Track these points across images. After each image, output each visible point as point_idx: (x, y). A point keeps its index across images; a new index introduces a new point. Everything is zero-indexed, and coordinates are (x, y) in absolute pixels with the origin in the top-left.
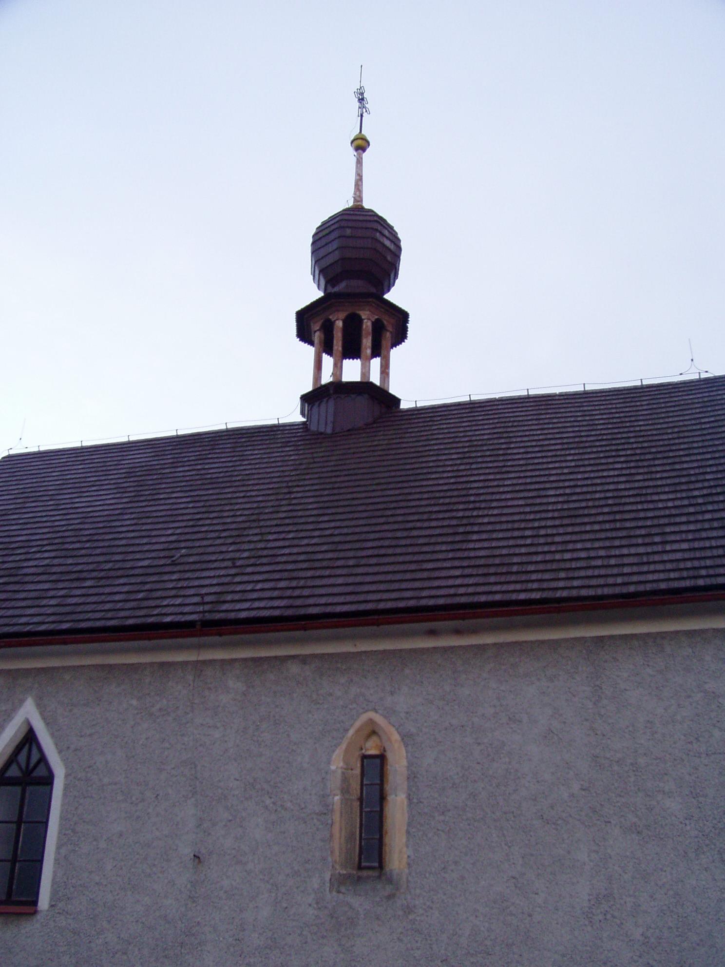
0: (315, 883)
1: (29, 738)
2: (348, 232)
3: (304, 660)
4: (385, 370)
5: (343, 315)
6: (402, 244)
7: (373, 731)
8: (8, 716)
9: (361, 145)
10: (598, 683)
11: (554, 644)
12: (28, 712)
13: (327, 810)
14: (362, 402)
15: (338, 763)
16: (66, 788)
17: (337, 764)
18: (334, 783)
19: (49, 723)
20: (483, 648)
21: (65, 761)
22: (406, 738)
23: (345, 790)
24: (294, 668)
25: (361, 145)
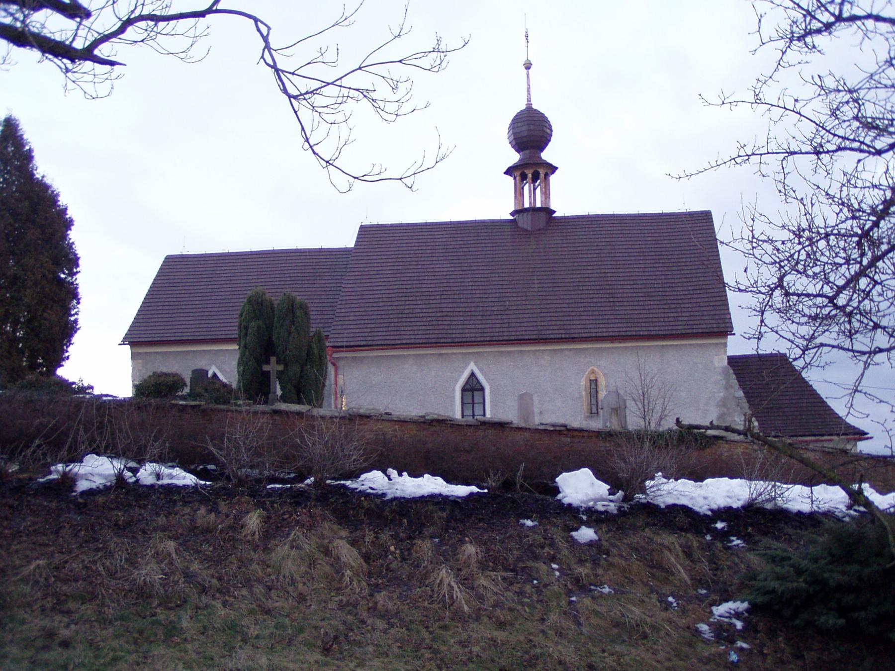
0: (579, 418)
1: (473, 375)
2: (532, 127)
3: (571, 350)
4: (546, 194)
5: (532, 171)
6: (553, 128)
7: (593, 372)
8: (465, 368)
9: (528, 66)
10: (250, 663)
11: (649, 347)
12: (472, 367)
13: (581, 397)
14: (543, 215)
15: (583, 382)
16: (491, 392)
17: (583, 383)
18: (583, 388)
19: (481, 370)
20: (628, 347)
21: (454, 390)
22: (604, 375)
23: (586, 391)
24: (567, 353)
25: (528, 66)
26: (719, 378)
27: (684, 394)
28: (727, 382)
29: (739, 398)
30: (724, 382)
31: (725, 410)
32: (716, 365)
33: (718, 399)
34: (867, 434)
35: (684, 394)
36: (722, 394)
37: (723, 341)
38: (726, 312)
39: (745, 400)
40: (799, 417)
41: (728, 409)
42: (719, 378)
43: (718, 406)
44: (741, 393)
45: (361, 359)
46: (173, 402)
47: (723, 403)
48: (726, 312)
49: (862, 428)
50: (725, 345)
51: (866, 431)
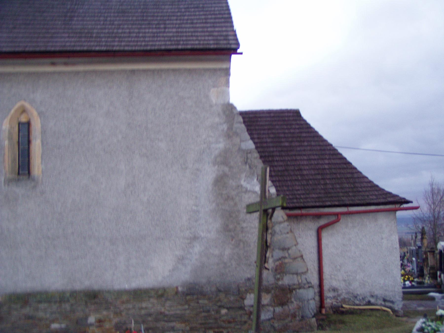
7: (24, 111)
17: (6, 126)
22: (40, 114)
23: (10, 139)
26: (217, 120)
27: (163, 145)
28: (230, 128)
29: (250, 152)
30: (225, 127)
31: (226, 169)
32: (214, 100)
33: (217, 152)
34: (408, 202)
35: (163, 145)
36: (221, 146)
37: (224, 66)
38: (230, 20)
39: (256, 155)
40: (322, 182)
41: (231, 168)
42: (217, 120)
43: (215, 163)
44: (250, 145)
45: (38, 75)
46: (391, 313)
47: (223, 159)
48: (230, 20)
49: (402, 195)
50: (227, 72)
51: (408, 198)
